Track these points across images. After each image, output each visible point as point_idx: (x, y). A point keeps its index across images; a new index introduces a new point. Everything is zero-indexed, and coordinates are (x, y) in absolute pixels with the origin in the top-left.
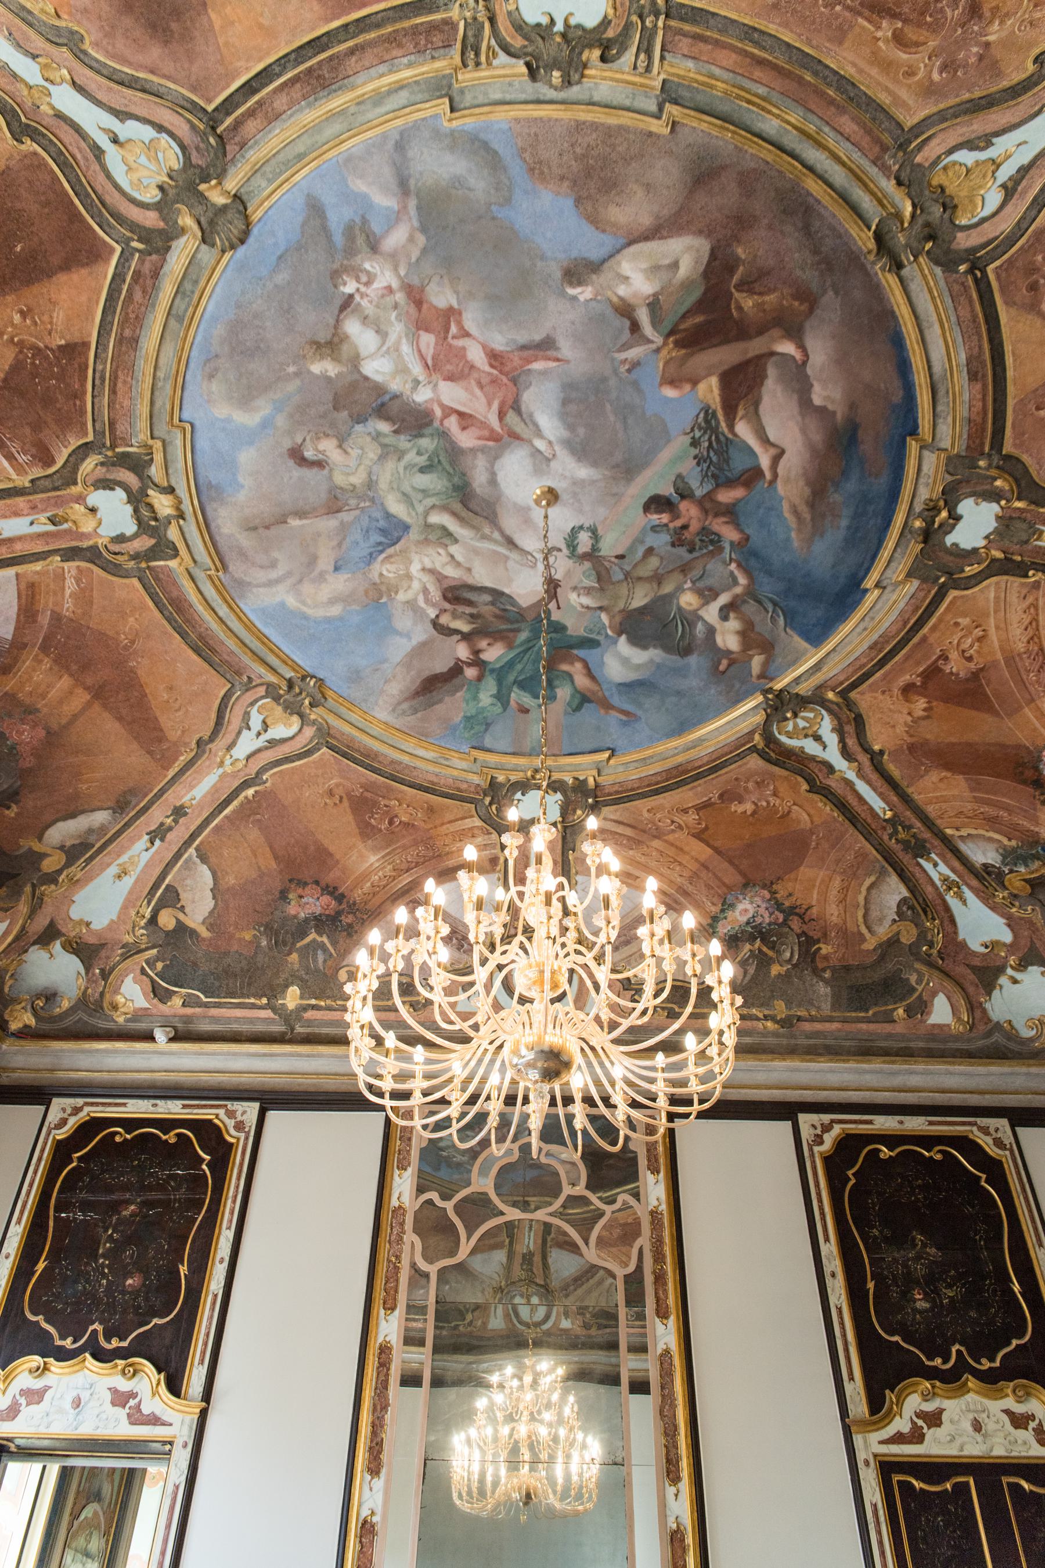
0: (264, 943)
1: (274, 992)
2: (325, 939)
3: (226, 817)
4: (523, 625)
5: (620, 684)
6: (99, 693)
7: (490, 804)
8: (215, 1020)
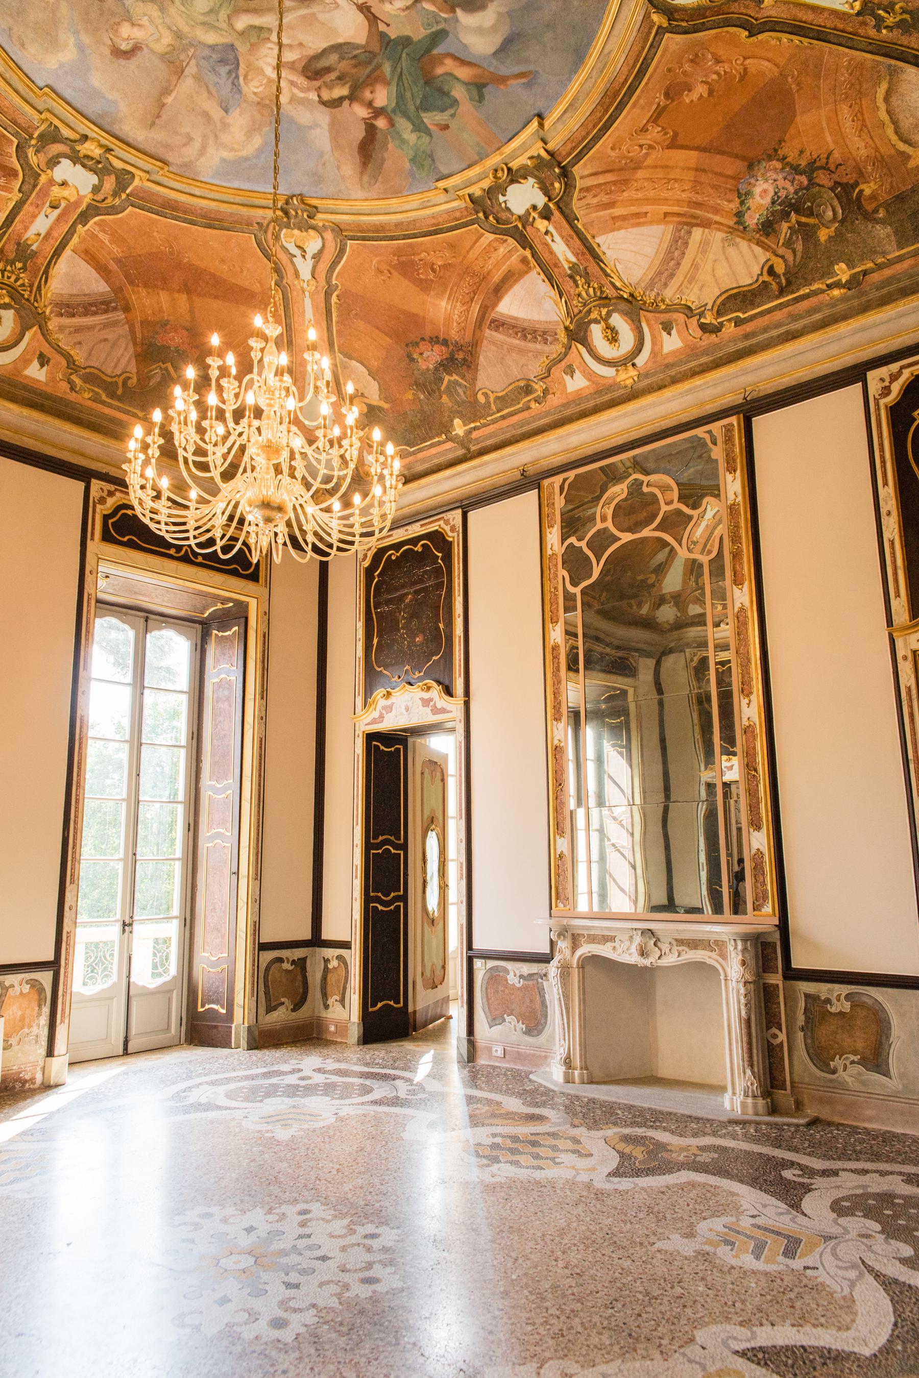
0: (422, 397)
1: (446, 428)
2: (455, 377)
3: (337, 322)
4: (378, 59)
5: (495, 54)
6: (188, 290)
7: (487, 217)
8: (423, 461)
